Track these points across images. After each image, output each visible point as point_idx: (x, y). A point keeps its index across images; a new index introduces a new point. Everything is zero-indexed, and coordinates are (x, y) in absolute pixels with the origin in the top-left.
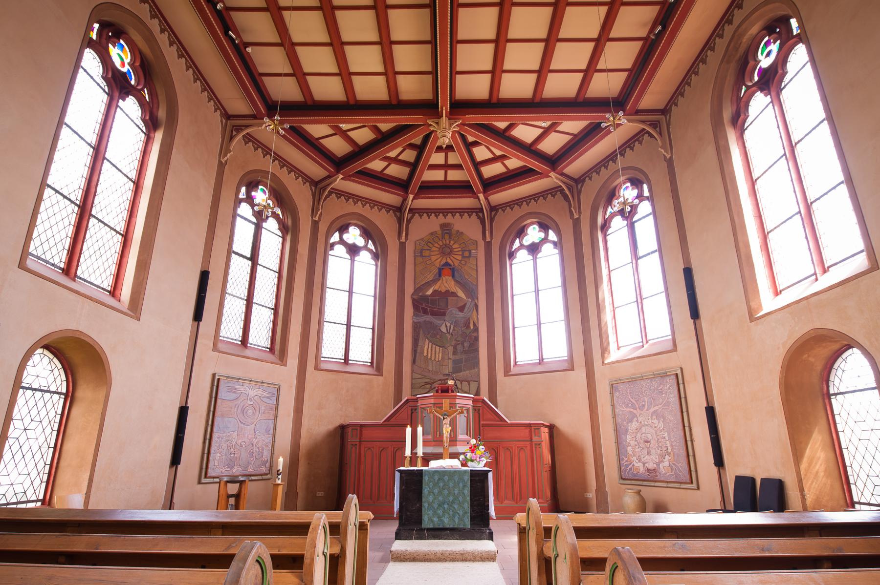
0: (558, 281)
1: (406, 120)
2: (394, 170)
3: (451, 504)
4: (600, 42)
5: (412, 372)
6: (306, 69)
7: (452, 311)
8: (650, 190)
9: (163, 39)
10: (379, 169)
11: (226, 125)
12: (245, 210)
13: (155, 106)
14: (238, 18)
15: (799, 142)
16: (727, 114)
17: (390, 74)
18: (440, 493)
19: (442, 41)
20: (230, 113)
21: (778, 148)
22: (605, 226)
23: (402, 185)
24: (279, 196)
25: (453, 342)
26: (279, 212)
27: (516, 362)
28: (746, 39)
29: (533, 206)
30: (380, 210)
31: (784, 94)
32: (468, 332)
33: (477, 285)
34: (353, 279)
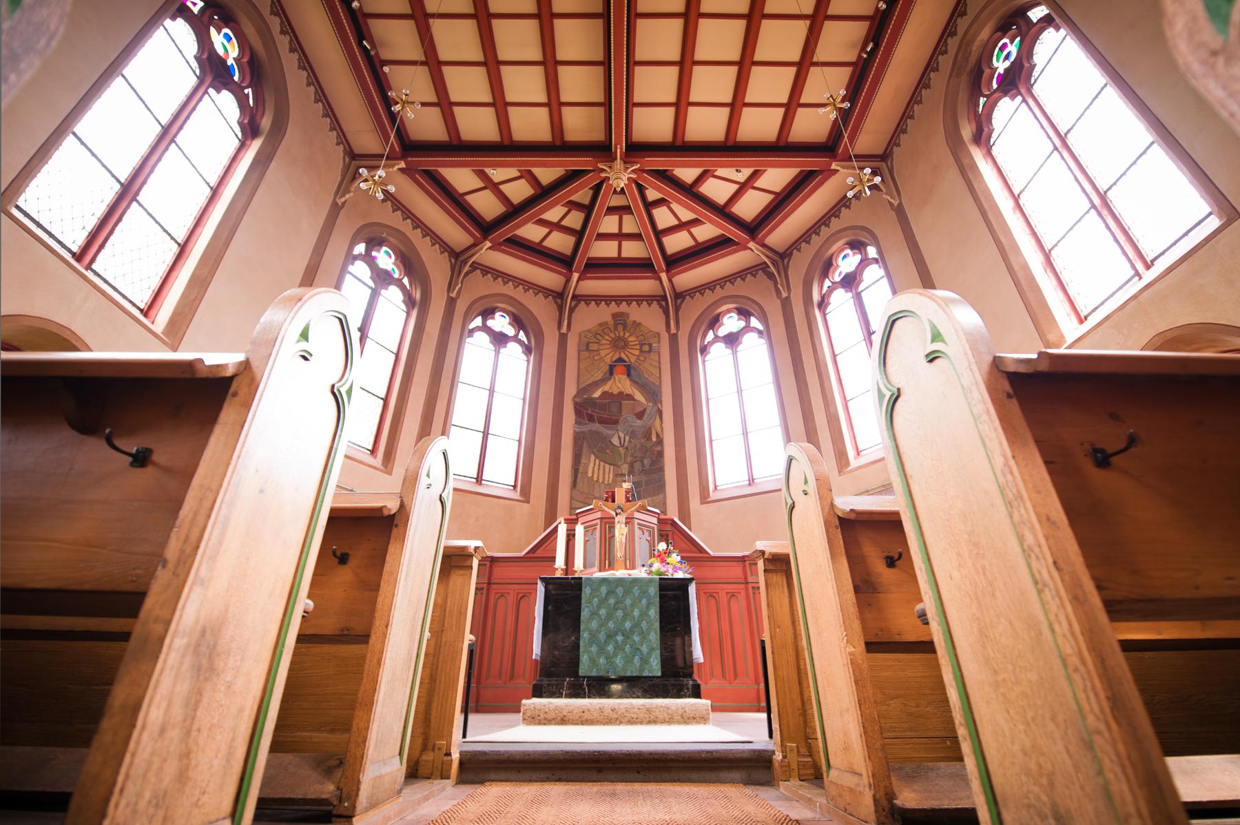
0: (769, 376)
1: (574, 164)
2: (560, 242)
3: (627, 635)
4: (804, 64)
5: (572, 498)
6: (453, 98)
7: (628, 418)
8: (880, 252)
9: (283, 42)
10: (537, 239)
11: (349, 164)
12: (360, 269)
13: (260, 113)
14: (376, 26)
15: (1069, 131)
16: (967, 132)
17: (555, 106)
18: (610, 616)
19: (617, 62)
20: (356, 152)
21: (1042, 144)
22: (823, 304)
23: (564, 262)
24: (409, 262)
25: (629, 459)
26: (406, 281)
27: (716, 487)
28: (976, 47)
29: (729, 289)
30: (536, 294)
31: (1037, 89)
32: (649, 445)
33: (660, 386)
34: (496, 379)
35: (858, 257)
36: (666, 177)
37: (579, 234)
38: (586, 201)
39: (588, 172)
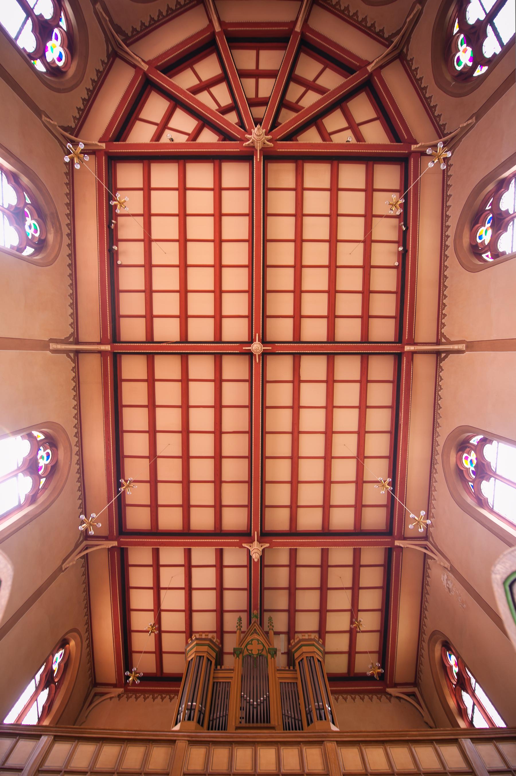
12: (491, 47)
13: (490, 193)
24: (446, 50)
35: (49, 59)
36: (225, 135)
37: (292, 77)
38: (284, 111)
39: (282, 139)
